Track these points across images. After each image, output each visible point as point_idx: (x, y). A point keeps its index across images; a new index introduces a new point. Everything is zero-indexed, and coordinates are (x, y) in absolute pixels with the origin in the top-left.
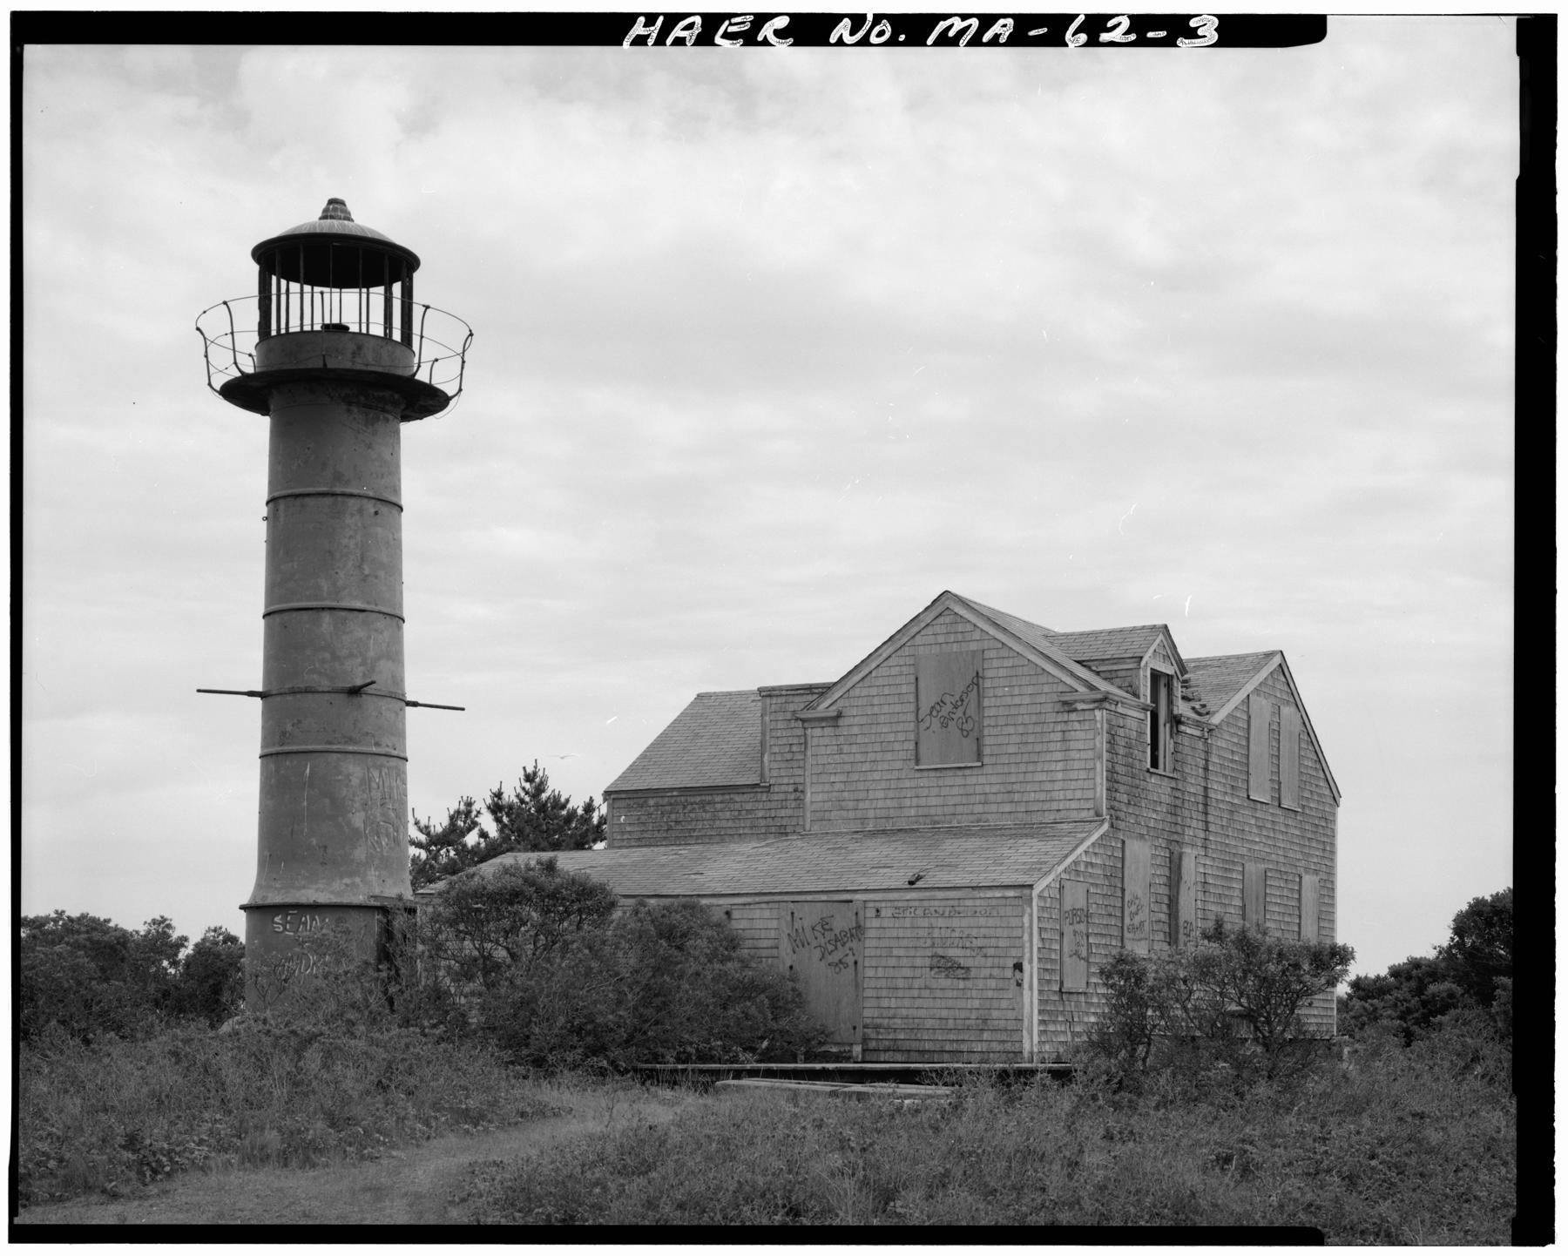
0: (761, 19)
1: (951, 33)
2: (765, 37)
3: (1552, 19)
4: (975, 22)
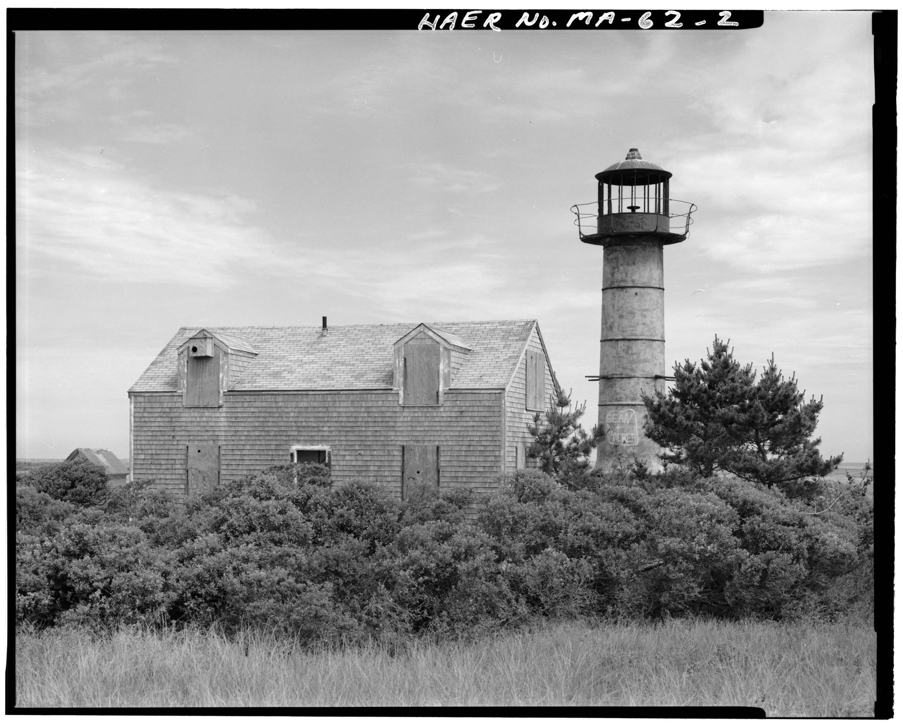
0: (486, 13)
2: (489, 24)
3: (10, 11)
4: (590, 14)
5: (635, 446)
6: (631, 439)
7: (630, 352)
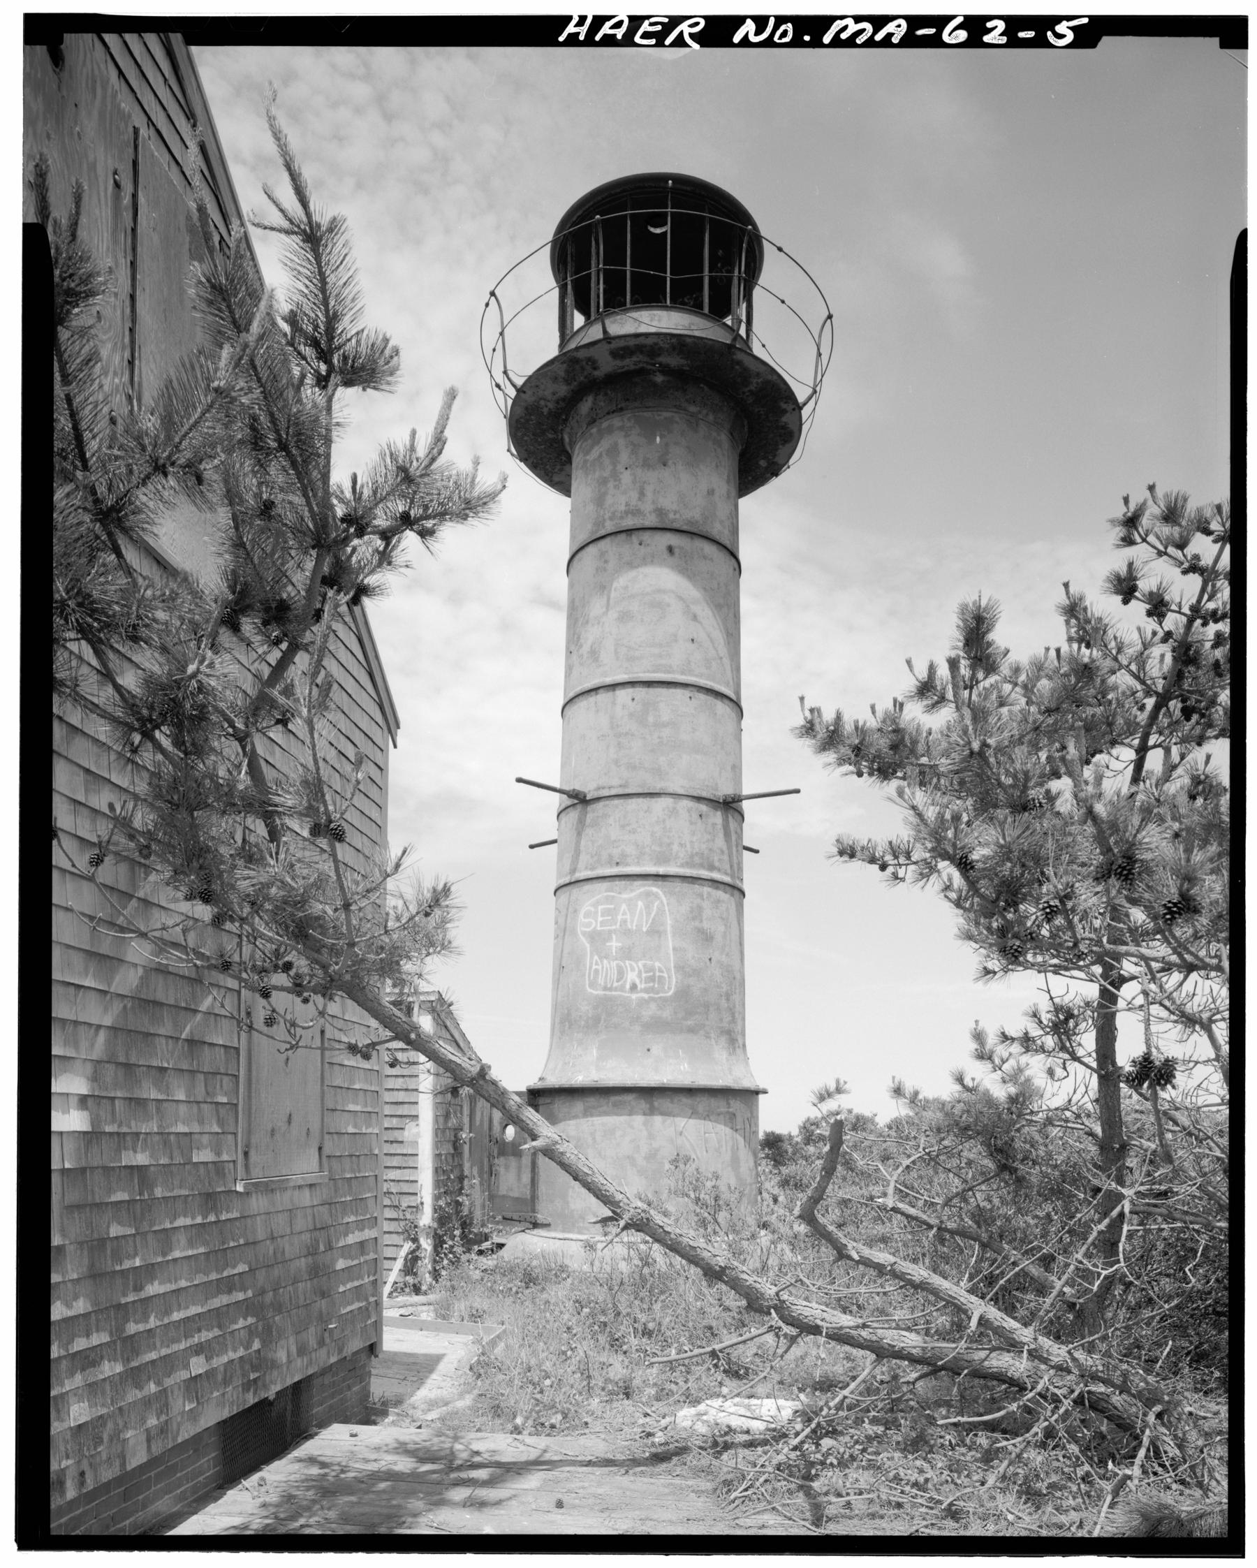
0: (675, 21)
1: (844, 36)
5: (665, 1000)
6: (652, 979)
7: (651, 719)
